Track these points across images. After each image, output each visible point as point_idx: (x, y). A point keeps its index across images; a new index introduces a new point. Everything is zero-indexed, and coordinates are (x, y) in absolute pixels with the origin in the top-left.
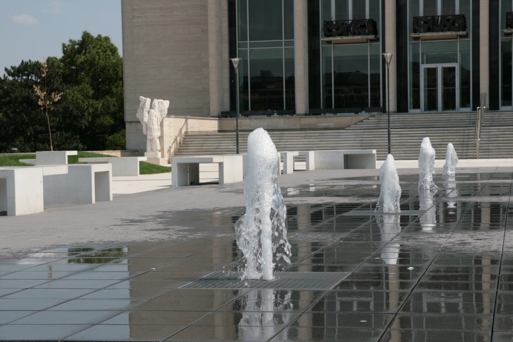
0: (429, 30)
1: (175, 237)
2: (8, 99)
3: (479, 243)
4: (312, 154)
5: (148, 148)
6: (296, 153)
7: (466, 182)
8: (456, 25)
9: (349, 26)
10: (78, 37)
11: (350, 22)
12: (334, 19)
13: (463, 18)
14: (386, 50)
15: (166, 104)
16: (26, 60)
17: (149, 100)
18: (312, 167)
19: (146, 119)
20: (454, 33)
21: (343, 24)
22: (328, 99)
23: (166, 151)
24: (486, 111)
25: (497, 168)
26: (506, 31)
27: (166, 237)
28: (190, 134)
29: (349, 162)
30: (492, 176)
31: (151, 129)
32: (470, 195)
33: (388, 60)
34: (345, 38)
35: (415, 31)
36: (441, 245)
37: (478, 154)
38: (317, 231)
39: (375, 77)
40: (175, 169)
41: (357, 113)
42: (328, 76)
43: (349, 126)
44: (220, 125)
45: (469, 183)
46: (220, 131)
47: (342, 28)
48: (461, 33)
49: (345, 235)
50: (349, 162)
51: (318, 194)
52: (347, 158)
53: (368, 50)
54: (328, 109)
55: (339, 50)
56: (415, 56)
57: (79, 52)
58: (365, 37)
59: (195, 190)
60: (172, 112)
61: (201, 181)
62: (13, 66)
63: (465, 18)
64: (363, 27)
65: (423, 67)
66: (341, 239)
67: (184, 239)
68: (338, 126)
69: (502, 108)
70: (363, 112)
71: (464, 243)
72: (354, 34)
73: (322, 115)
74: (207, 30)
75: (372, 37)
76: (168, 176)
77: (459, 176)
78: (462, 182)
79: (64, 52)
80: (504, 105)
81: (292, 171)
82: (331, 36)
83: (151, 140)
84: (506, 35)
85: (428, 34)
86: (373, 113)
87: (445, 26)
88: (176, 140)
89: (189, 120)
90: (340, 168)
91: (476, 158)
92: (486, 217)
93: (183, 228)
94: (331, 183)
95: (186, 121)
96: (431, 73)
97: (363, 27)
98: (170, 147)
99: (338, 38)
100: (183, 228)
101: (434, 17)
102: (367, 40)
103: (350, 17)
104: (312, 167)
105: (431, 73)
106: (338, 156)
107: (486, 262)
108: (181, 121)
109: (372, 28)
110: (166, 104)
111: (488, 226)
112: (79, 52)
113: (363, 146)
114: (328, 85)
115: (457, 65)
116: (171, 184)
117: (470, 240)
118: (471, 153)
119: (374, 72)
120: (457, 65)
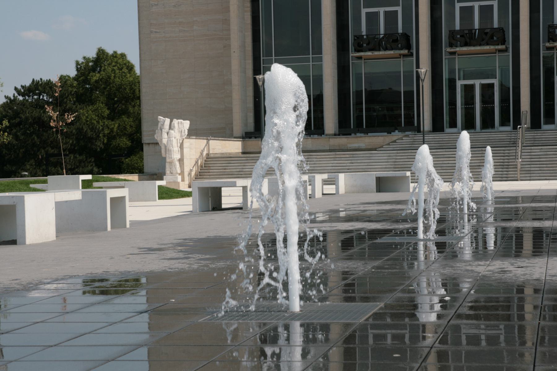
0: (466, 44)
1: (195, 266)
2: (18, 120)
3: (520, 271)
4: (342, 177)
5: (168, 172)
6: (325, 176)
7: (506, 206)
8: (495, 38)
9: (381, 40)
10: (92, 54)
11: (381, 36)
12: (364, 33)
13: (501, 31)
14: (421, 66)
15: (187, 124)
16: (37, 78)
17: (168, 121)
18: (342, 190)
19: (165, 141)
20: (492, 47)
21: (375, 38)
22: (359, 119)
23: (186, 174)
24: (527, 129)
25: (539, 191)
26: (548, 45)
27: (186, 266)
28: (212, 156)
29: (382, 185)
30: (534, 199)
31: (170, 151)
32: (511, 220)
33: (422, 76)
34: (376, 53)
35: (451, 45)
36: (480, 273)
37: (519, 176)
38: (348, 259)
39: (409, 95)
40: (196, 194)
41: (389, 132)
42: (358, 94)
43: (382, 147)
44: (244, 147)
45: (508, 208)
46: (243, 153)
47: (372, 43)
48: (500, 47)
49: (377, 263)
50: (382, 185)
51: (349, 219)
52: (379, 180)
53: (401, 66)
54: (359, 128)
55: (370, 65)
56: (452, 71)
57: (93, 69)
58: (398, 52)
59: (217, 216)
60: (193, 133)
61: (224, 206)
62: (23, 85)
63: (504, 31)
64: (396, 41)
65: (460, 83)
66: (373, 268)
67: (205, 268)
68: (369, 147)
69: (544, 127)
70: (397, 131)
71: (504, 272)
72: (386, 49)
73: (353, 135)
74: (230, 46)
75: (405, 52)
76: (188, 201)
77: (499, 199)
78: (502, 206)
79: (78, 70)
80: (546, 123)
81: (321, 195)
82: (362, 51)
83: (171, 163)
84: (548, 49)
85: (465, 49)
86: (407, 133)
87: (483, 40)
88: (197, 162)
89: (211, 142)
90: (371, 192)
91: (517, 180)
92: (528, 243)
93: (204, 257)
94: (362, 208)
95: (208, 143)
96: (469, 90)
97: (396, 41)
98: (191, 170)
99: (369, 53)
100: (204, 257)
101: (471, 30)
102: (400, 55)
103: (382, 31)
104: (342, 190)
105: (469, 90)
106: (370, 178)
107: (528, 291)
108: (202, 143)
109: (405, 42)
110: (187, 124)
111: (530, 252)
112: (93, 69)
113: (395, 169)
114: (359, 103)
115: (496, 82)
116: (191, 210)
117: (511, 268)
118: (511, 174)
119: (408, 89)
120: (496, 82)
